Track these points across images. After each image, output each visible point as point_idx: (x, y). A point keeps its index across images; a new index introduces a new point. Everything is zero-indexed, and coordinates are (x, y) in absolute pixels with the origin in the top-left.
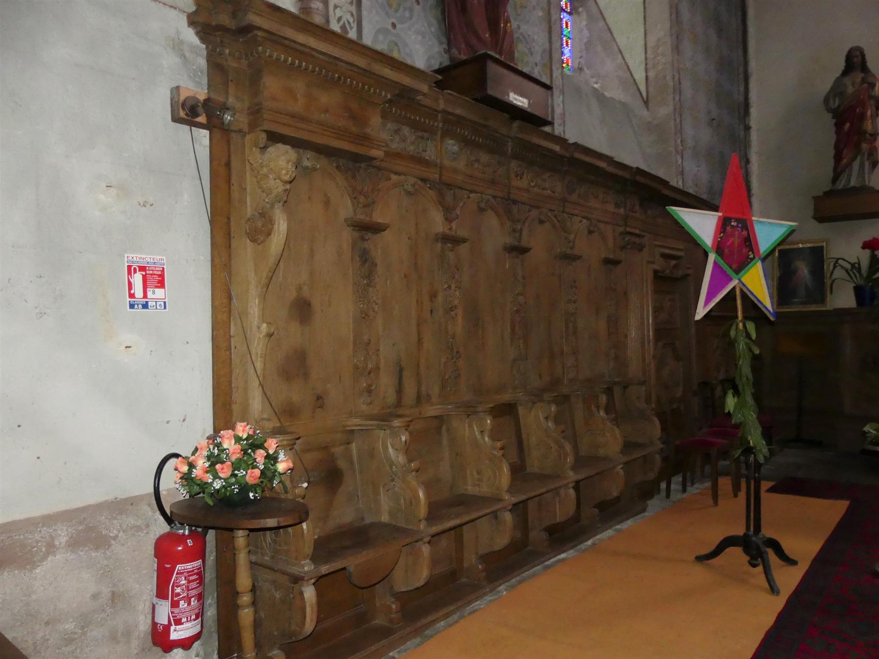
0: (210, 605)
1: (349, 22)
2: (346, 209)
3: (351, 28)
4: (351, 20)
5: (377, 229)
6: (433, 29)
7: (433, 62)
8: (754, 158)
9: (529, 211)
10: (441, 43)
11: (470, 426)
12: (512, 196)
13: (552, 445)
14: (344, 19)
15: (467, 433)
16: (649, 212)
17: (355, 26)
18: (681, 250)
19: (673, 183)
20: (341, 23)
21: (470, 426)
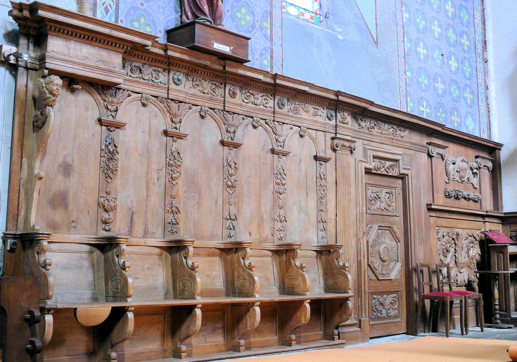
0: (314, 281)
1: (110, 5)
2: (94, 113)
3: (111, 8)
4: (112, 3)
5: (119, 126)
6: (171, 4)
7: (170, 24)
8: (492, 86)
9: (243, 119)
10: (177, 12)
11: (180, 255)
12: (171, 96)
13: (247, 277)
14: (107, 3)
15: (178, 259)
16: (363, 124)
17: (114, 7)
18: (400, 154)
19: (448, 126)
20: (105, 5)
21: (180, 255)
